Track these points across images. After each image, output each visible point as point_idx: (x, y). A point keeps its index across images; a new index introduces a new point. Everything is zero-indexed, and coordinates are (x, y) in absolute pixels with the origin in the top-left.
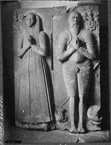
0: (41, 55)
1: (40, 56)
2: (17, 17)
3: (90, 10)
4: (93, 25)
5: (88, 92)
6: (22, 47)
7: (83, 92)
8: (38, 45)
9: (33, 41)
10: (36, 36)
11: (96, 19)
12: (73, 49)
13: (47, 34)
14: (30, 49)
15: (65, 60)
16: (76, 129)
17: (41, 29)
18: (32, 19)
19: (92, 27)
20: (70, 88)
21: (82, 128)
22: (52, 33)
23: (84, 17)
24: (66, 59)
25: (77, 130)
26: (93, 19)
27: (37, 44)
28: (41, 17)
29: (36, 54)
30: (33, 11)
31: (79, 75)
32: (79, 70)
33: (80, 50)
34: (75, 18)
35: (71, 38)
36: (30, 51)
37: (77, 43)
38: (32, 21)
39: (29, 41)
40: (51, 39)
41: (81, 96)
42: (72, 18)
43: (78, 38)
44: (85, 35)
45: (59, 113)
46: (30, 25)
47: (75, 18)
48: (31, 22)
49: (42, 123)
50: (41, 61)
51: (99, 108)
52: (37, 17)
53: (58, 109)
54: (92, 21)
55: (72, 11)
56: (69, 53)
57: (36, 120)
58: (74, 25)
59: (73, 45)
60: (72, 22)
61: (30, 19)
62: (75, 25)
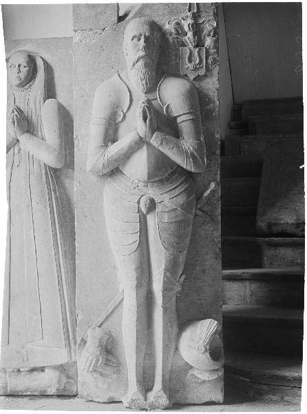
0: (39, 162)
1: (43, 165)
3: (189, 14)
4: (197, 62)
5: (182, 274)
7: (163, 275)
10: (33, 111)
11: (209, 42)
12: (133, 135)
13: (65, 106)
14: (16, 147)
15: (114, 171)
17: (50, 92)
19: (195, 69)
20: (124, 261)
21: (162, 392)
22: (43, 59)
23: (171, 35)
24: (114, 171)
25: (146, 400)
26: (200, 44)
28: (49, 62)
29: (31, 160)
30: (30, 48)
31: (152, 220)
32: (152, 205)
33: (155, 141)
34: (139, 39)
35: (129, 103)
36: (16, 151)
37: (145, 119)
38: (24, 70)
39: (14, 123)
41: (158, 287)
42: (132, 40)
43: (149, 101)
44: (173, 94)
45: (90, 344)
49: (42, 369)
50: (44, 179)
52: (40, 63)
53: (88, 331)
54: (197, 50)
56: (122, 149)
57: (25, 359)
59: (134, 126)
60: (132, 50)
61: (19, 66)
62: (141, 63)
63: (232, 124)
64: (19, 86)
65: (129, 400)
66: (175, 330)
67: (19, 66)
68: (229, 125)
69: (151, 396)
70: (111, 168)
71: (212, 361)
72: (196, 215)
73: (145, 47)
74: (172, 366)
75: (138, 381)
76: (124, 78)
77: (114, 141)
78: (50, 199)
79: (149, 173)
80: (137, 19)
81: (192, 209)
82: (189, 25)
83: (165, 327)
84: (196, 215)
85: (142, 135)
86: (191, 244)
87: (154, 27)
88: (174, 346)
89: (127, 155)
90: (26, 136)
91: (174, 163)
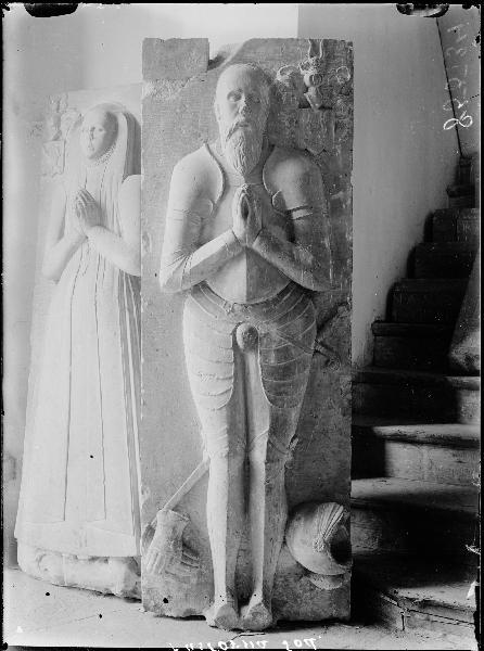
2: (58, 123)
3: (311, 60)
5: (294, 438)
6: (61, 235)
8: (116, 231)
9: (95, 212)
14: (85, 247)
16: (232, 611)
18: (101, 130)
27: (110, 226)
31: (254, 362)
34: (238, 98)
38: (100, 135)
40: (268, 250)
41: (259, 456)
46: (92, 153)
47: (243, 99)
48: (93, 142)
51: (337, 515)
52: (122, 122)
55: (229, 64)
58: (235, 130)
59: (232, 224)
60: (226, 113)
62: (239, 133)
63: (454, 189)
64: (92, 158)
65: (214, 617)
66: (282, 517)
67: (93, 129)
68: (448, 190)
69: (247, 611)
70: (194, 283)
71: (334, 563)
72: (316, 351)
73: (245, 110)
74: (277, 567)
75: (228, 589)
76: (215, 152)
77: (199, 245)
78: (122, 321)
79: (248, 293)
80: (236, 66)
81: (310, 344)
82: (311, 77)
83: (269, 512)
84: (316, 351)
85: (239, 234)
86: (308, 393)
87: (258, 77)
88: (280, 539)
89: (220, 266)
90: (97, 230)
91: (285, 278)
